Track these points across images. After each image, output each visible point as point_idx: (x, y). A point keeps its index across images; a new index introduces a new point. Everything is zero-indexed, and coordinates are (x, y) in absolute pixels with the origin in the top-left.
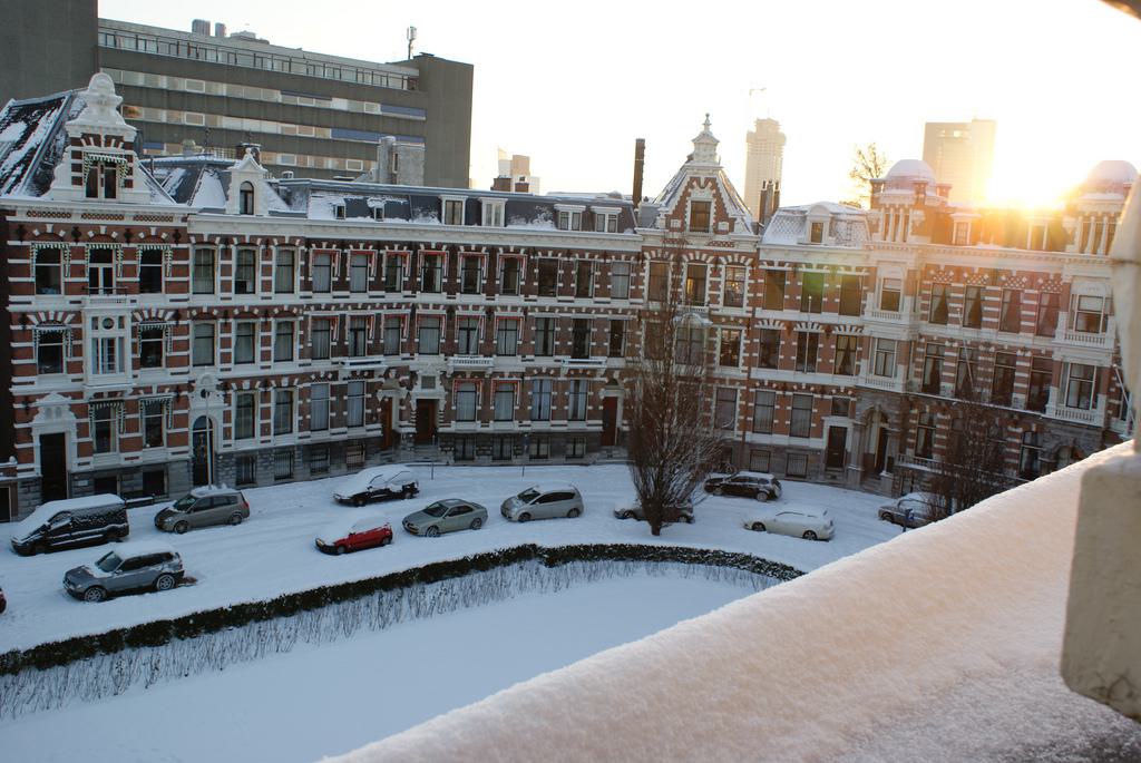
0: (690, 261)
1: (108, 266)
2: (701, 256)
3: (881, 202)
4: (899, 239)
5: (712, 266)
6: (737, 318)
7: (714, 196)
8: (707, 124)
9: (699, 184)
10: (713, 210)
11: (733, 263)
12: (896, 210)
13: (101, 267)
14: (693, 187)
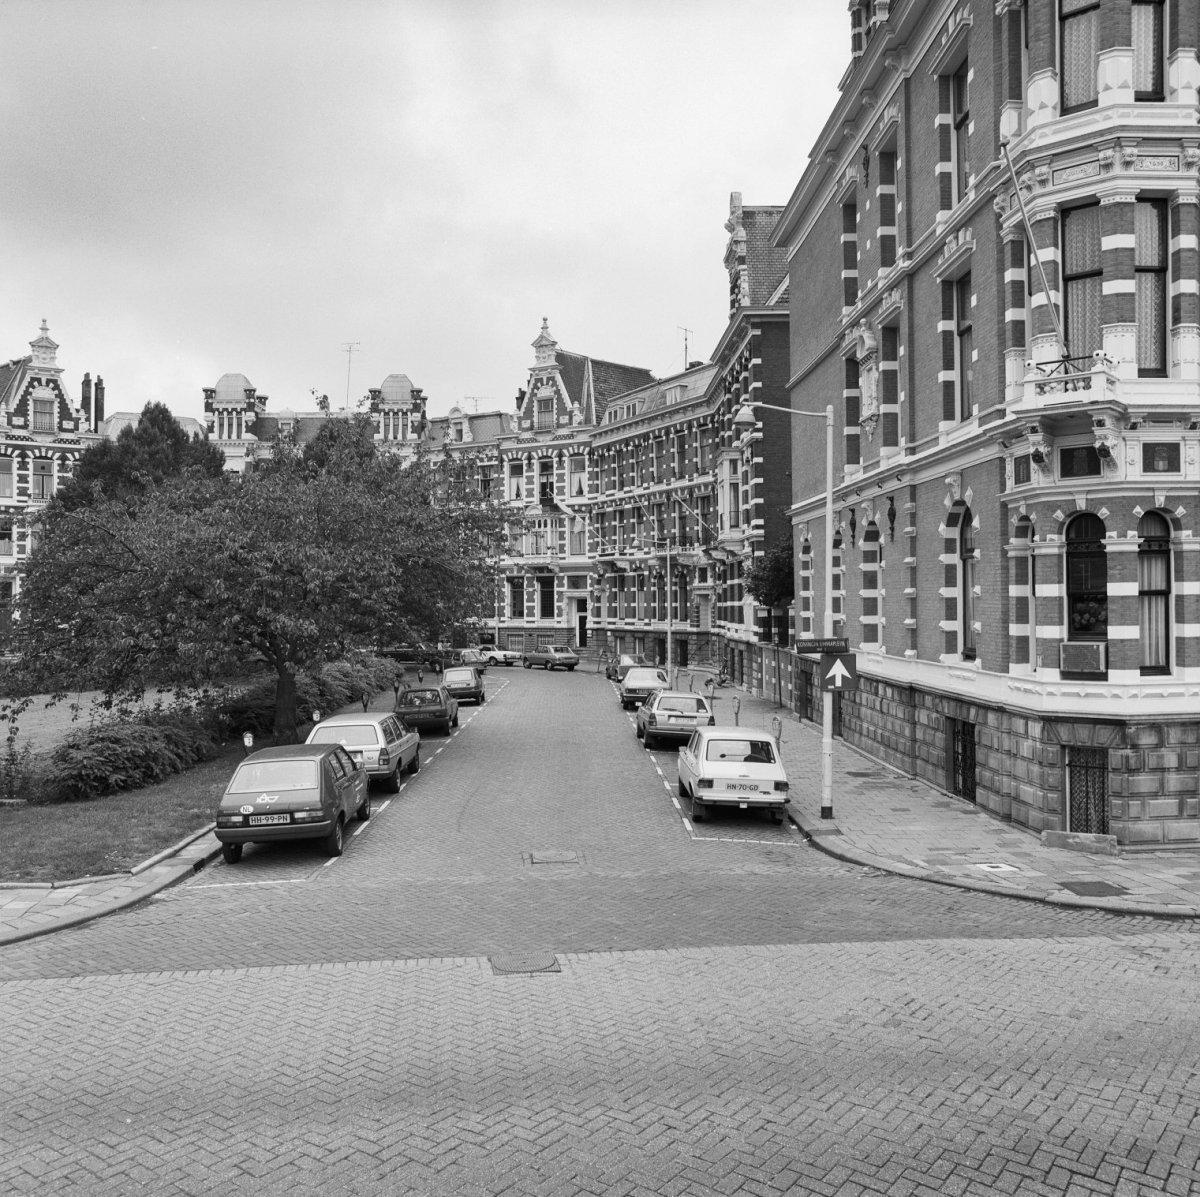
0: (36, 458)
2: (47, 453)
3: (214, 406)
4: (234, 436)
5: (60, 462)
6: (581, 506)
7: (56, 396)
8: (545, 328)
9: (40, 383)
10: (56, 410)
11: (41, 457)
12: (229, 413)
14: (34, 387)
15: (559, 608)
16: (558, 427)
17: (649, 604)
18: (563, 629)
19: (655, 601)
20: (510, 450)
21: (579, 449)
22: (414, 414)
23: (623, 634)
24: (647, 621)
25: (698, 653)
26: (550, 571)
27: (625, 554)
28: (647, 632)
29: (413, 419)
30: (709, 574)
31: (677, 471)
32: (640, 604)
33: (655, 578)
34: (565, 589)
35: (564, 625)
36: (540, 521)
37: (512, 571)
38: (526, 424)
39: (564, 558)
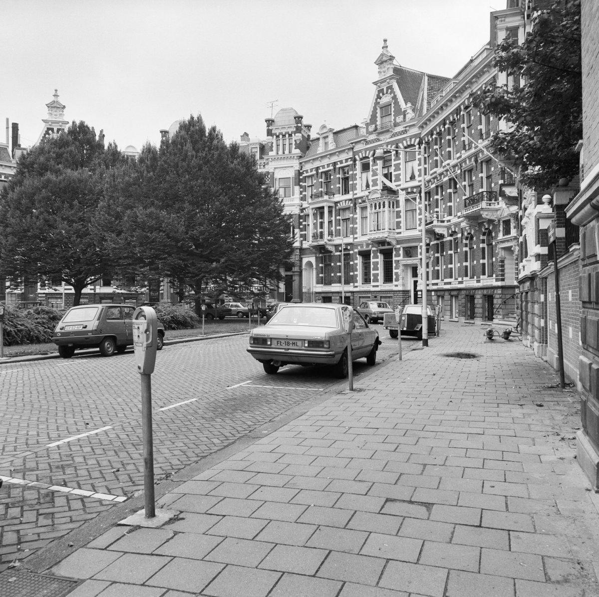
1: (399, 333)
2: (411, 141)
3: (273, 132)
6: (412, 188)
8: (385, 47)
13: (399, 336)
15: (397, 274)
16: (395, 126)
17: (462, 264)
18: (399, 291)
19: (466, 261)
20: (360, 151)
21: (411, 142)
22: (296, 134)
23: (442, 293)
24: (460, 279)
25: (503, 307)
26: (389, 244)
27: (443, 222)
28: (460, 290)
29: (296, 138)
30: (512, 225)
31: (484, 131)
32: (455, 266)
33: (467, 238)
34: (401, 258)
35: (400, 288)
36: (380, 203)
37: (362, 247)
38: (372, 128)
39: (400, 233)
